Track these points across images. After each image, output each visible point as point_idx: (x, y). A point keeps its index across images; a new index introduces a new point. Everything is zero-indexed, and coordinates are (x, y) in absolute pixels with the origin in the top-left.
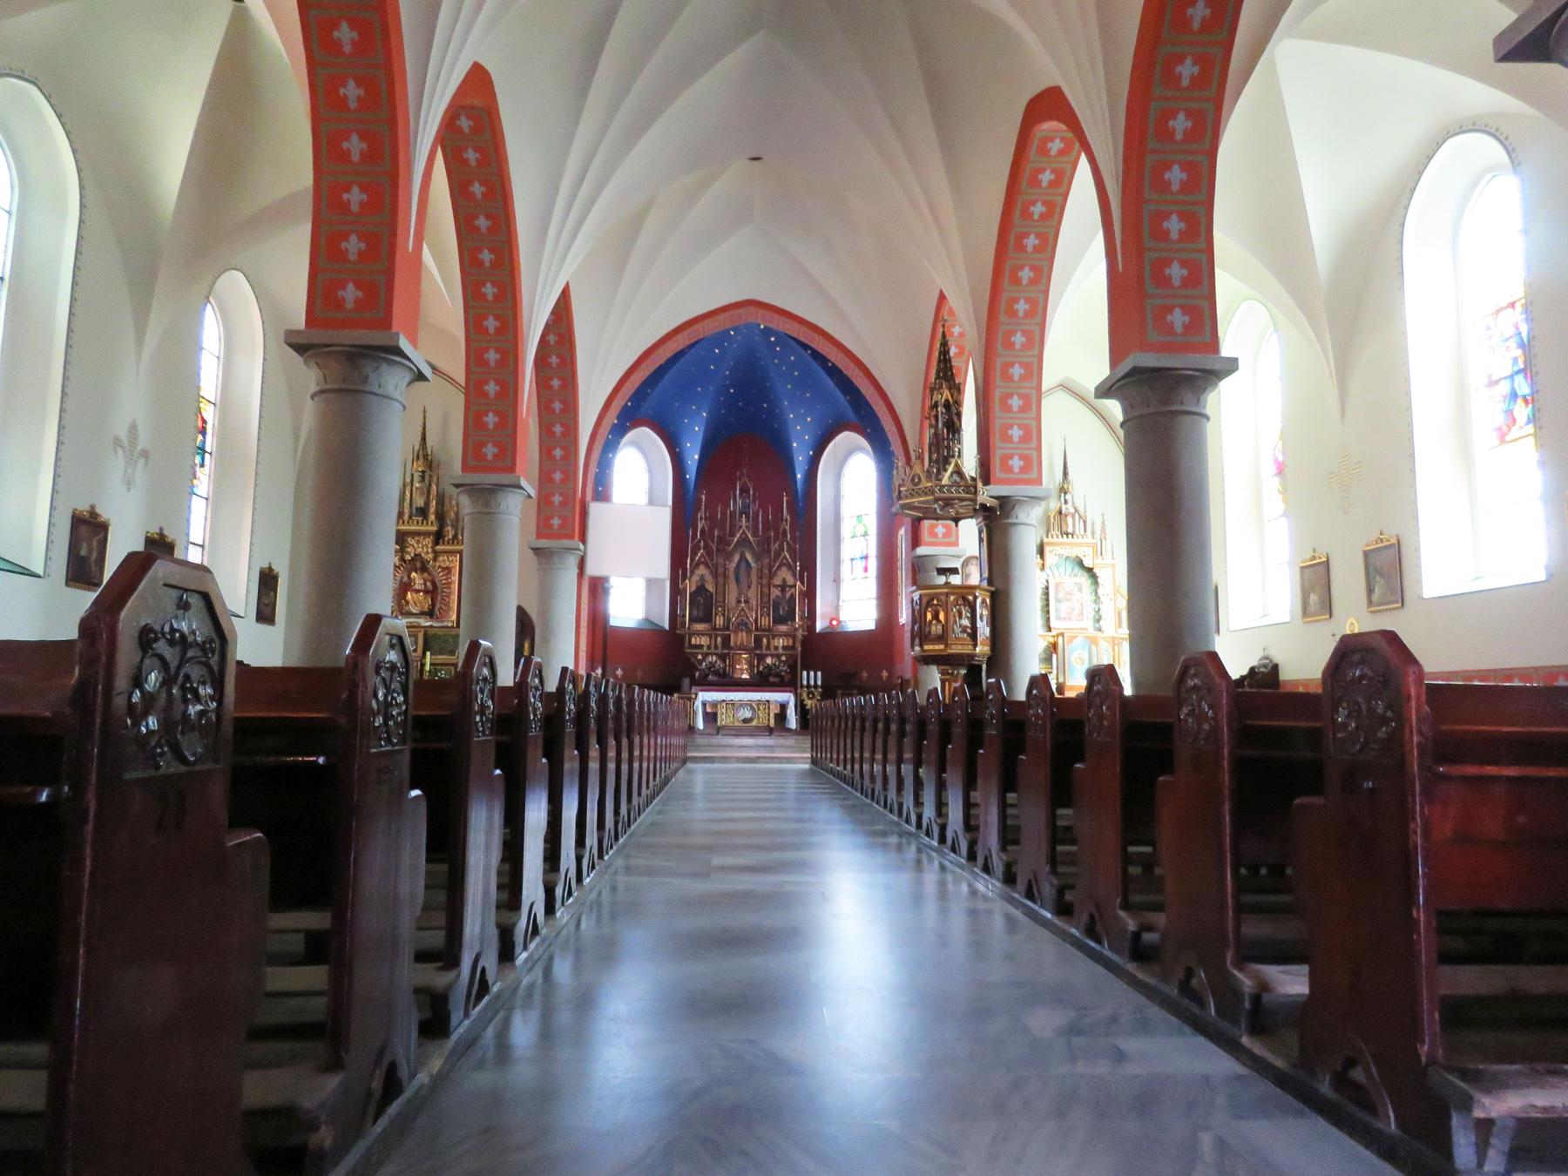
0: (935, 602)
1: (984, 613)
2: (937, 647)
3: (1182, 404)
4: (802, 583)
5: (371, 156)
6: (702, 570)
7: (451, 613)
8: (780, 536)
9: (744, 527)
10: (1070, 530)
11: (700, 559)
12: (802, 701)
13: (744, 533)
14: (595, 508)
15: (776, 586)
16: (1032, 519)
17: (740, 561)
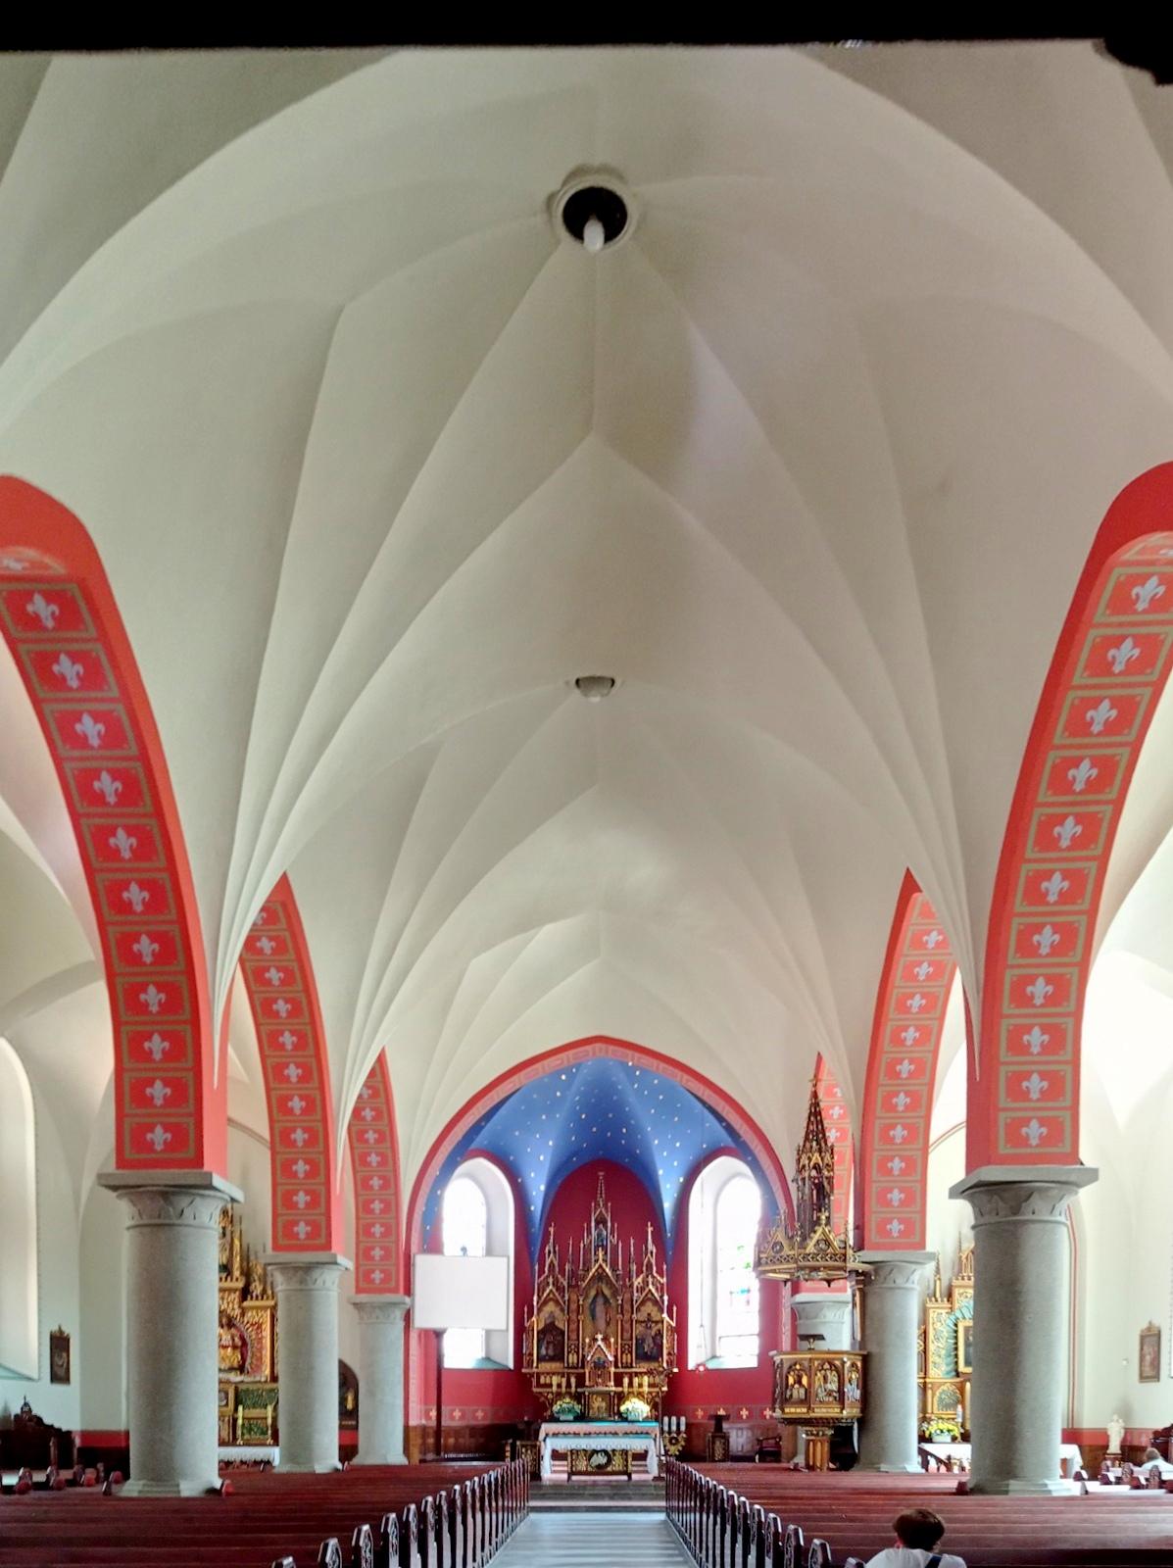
0: (798, 1367)
1: (853, 1376)
2: (798, 1410)
3: (1033, 1213)
4: (671, 1316)
5: (171, 1006)
8: (644, 1269)
11: (548, 1294)
13: (601, 1266)
14: (423, 1263)
16: (913, 1283)
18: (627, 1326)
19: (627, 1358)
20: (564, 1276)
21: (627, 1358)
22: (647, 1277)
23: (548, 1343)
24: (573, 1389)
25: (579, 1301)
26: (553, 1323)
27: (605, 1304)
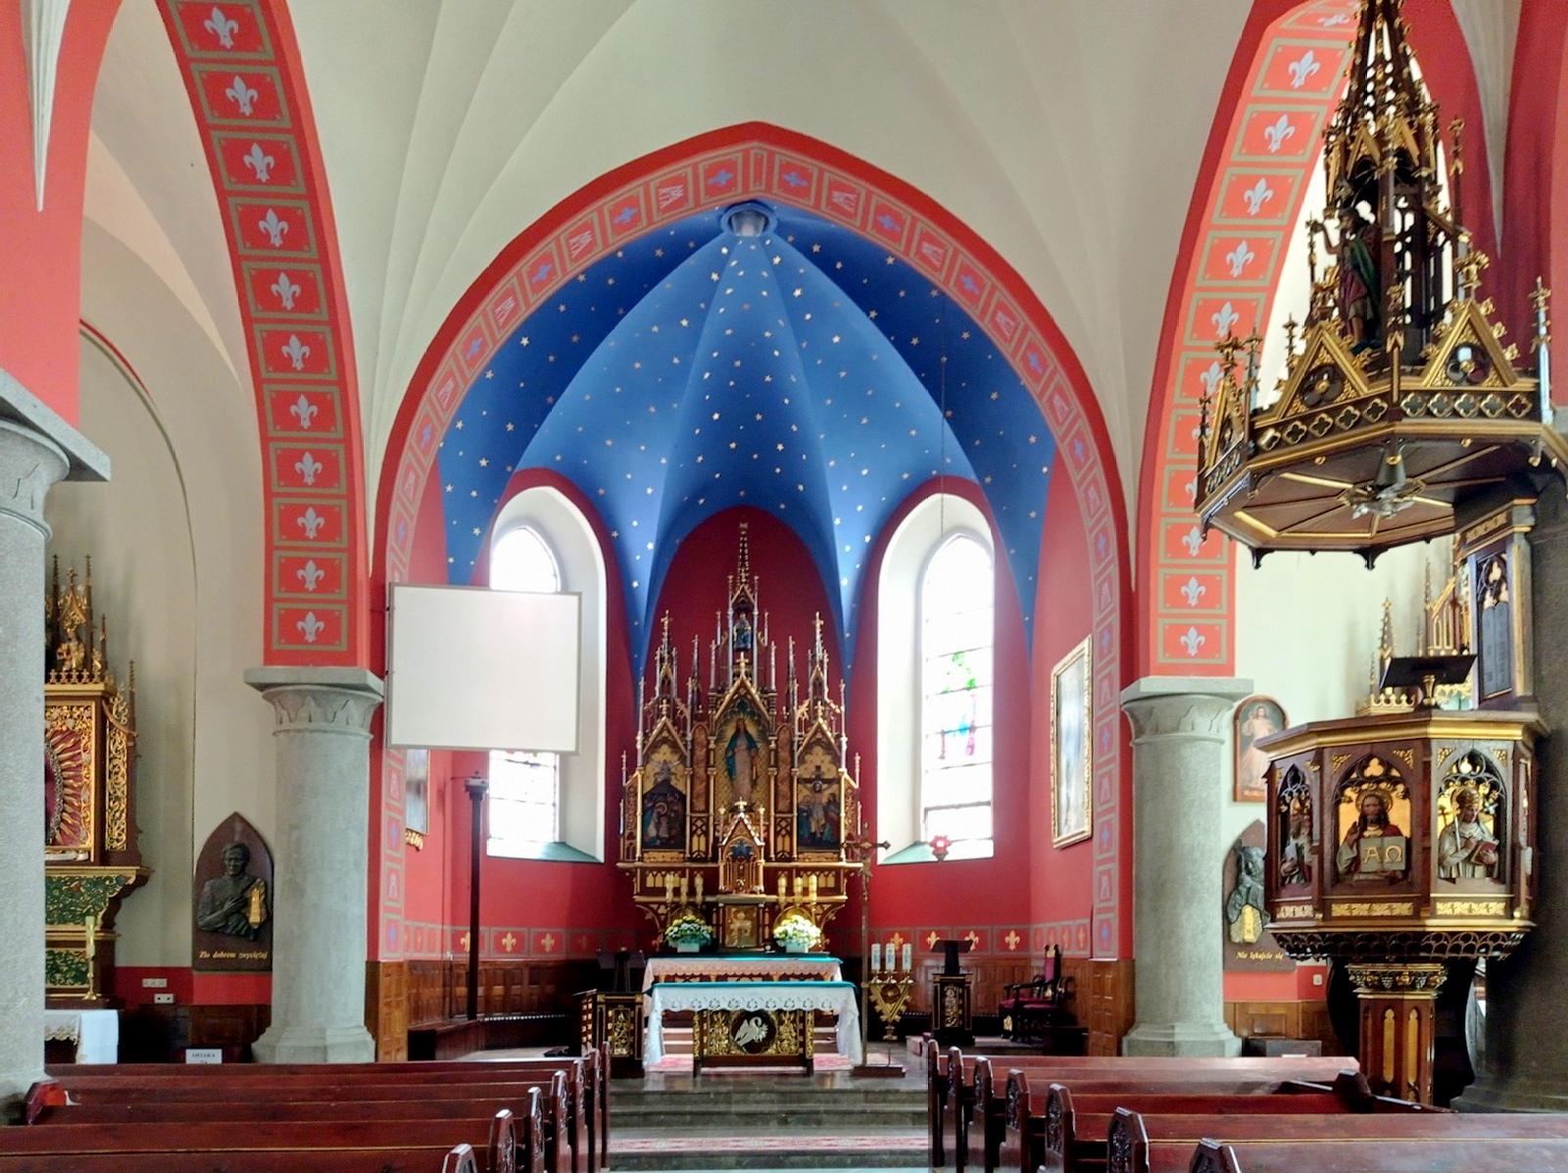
0: (1375, 769)
6: (664, 753)
7: (83, 834)
9: (743, 675)
11: (661, 732)
12: (872, 1005)
15: (802, 781)
17: (735, 737)
18: (784, 788)
19: (783, 844)
20: (684, 701)
21: (783, 844)
22: (815, 704)
23: (660, 816)
24: (699, 898)
25: (708, 742)
26: (667, 782)
27: (749, 748)
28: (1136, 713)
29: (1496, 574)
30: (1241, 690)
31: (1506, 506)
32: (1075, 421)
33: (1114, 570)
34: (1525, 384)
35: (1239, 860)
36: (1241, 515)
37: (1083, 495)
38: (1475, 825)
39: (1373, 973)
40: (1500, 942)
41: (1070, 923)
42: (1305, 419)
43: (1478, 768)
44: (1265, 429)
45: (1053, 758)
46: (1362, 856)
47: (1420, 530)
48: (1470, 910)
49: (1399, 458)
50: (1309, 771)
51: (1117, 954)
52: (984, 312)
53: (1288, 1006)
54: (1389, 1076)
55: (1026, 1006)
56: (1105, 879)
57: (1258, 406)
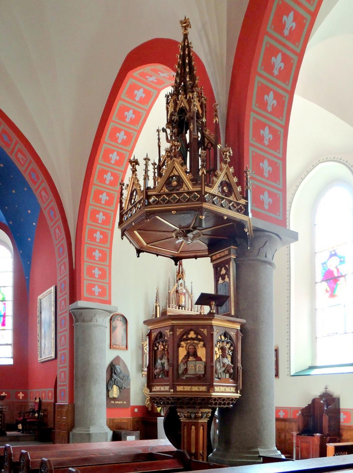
0: (192, 335)
10: (183, 304)
28: (75, 314)
29: (223, 271)
30: (114, 310)
31: (228, 248)
32: (50, 202)
33: (66, 260)
34: (243, 201)
35: (112, 369)
36: (136, 232)
37: (53, 231)
38: (226, 359)
39: (188, 412)
40: (233, 402)
41: (39, 390)
42: (167, 195)
43: (226, 338)
44: (151, 196)
45: (38, 329)
46: (188, 368)
47: (194, 254)
48: (225, 390)
49: (204, 217)
50: (168, 332)
51: (68, 401)
52: (12, 152)
53: (128, 419)
54: (193, 451)
55: (28, 420)
56: (63, 374)
57: (149, 186)
